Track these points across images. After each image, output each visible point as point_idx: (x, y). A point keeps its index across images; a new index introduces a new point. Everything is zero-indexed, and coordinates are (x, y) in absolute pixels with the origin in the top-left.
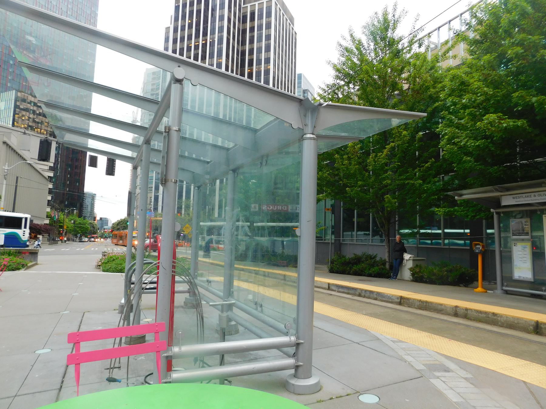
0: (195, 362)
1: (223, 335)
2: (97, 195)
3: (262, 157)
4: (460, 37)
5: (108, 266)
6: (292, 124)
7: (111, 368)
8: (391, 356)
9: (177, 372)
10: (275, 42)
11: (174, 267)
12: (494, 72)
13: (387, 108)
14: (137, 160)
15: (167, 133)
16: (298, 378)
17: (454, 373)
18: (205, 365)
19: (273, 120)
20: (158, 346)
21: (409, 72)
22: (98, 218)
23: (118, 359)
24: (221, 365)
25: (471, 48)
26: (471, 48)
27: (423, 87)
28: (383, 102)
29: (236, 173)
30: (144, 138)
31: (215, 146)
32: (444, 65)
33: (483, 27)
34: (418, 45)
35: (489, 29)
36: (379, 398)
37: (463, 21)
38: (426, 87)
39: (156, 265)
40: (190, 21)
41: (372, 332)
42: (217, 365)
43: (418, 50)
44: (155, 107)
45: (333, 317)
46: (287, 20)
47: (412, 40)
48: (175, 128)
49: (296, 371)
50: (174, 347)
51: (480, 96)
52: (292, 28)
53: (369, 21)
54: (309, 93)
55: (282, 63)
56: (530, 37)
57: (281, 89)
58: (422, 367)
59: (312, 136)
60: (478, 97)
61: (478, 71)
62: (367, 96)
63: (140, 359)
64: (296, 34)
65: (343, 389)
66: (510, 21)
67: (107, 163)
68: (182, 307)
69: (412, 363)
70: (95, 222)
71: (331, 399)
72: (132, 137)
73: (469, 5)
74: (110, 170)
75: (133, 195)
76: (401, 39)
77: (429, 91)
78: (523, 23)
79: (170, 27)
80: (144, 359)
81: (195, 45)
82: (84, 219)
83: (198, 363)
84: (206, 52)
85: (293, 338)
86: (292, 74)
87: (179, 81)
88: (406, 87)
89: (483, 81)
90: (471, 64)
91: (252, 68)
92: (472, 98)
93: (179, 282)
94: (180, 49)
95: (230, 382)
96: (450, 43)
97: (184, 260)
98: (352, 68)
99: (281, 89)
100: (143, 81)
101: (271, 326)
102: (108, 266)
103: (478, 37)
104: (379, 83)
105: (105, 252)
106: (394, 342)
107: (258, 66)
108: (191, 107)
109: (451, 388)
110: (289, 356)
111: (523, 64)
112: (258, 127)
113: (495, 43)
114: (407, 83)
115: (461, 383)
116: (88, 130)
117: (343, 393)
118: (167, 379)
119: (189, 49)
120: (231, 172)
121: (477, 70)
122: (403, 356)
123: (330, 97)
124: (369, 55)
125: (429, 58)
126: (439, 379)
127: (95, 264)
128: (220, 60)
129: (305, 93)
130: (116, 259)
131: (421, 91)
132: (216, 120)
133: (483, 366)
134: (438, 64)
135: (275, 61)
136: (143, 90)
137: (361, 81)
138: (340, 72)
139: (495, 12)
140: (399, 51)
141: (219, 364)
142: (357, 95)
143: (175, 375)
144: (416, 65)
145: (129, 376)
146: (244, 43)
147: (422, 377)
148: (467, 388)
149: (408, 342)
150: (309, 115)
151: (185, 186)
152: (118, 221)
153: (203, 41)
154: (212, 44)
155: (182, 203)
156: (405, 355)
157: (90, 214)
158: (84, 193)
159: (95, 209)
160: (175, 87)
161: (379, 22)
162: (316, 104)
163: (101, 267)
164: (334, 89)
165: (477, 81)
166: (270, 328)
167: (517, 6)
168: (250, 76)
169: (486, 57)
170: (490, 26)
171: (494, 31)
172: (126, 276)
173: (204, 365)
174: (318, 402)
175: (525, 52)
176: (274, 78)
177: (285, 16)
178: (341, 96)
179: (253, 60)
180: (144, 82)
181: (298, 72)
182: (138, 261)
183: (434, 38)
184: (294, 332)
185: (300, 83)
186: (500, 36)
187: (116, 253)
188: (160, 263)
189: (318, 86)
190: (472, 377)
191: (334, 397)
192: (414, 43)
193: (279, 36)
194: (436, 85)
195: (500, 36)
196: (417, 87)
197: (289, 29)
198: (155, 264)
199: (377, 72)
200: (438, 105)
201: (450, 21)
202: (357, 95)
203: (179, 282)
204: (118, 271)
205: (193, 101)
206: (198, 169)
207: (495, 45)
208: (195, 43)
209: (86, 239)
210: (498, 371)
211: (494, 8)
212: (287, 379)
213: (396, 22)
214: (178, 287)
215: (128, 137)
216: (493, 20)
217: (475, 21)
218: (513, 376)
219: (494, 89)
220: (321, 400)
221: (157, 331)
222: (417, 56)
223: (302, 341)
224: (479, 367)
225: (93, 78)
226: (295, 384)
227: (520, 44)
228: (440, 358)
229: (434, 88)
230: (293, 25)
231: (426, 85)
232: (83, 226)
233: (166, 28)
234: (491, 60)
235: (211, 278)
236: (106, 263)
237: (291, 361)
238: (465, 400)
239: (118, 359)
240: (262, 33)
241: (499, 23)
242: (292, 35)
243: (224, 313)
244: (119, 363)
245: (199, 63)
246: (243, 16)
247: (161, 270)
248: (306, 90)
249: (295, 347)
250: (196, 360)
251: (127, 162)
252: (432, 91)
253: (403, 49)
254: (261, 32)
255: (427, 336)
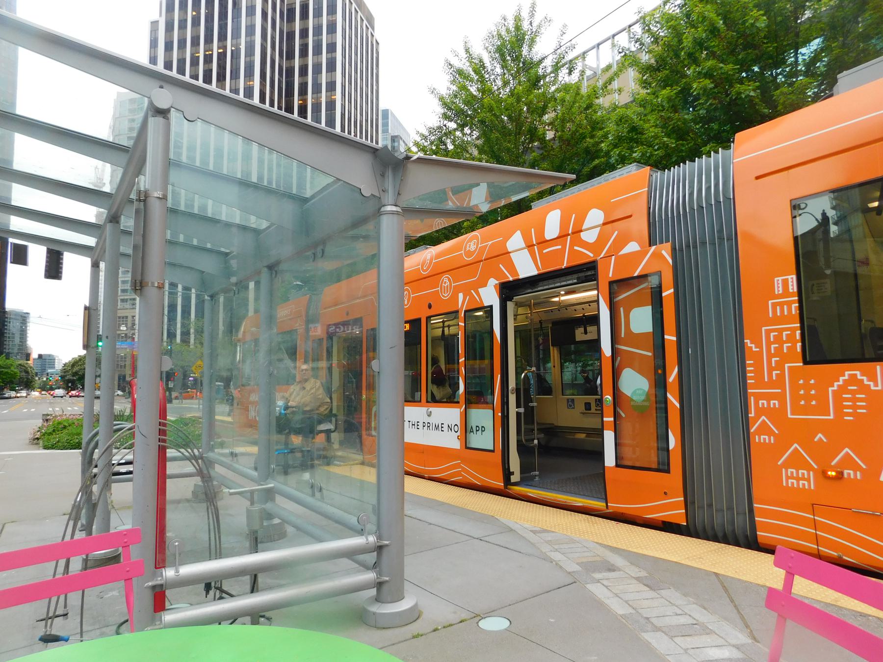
0: (207, 592)
1: (255, 545)
2: (31, 315)
3: (315, 245)
4: (628, 60)
5: (54, 439)
6: (361, 188)
7: (49, 618)
8: (530, 555)
9: (173, 611)
10: (344, 56)
11: (162, 432)
12: (677, 114)
13: (523, 166)
14: (98, 251)
15: (142, 203)
16: (383, 603)
17: (622, 572)
18: (224, 595)
19: (332, 182)
20: (128, 569)
21: (555, 112)
22: (34, 355)
23: (62, 597)
24: (252, 591)
25: (645, 78)
26: (645, 78)
27: (575, 135)
28: (517, 157)
29: (274, 272)
30: (108, 212)
31: (244, 228)
32: (604, 102)
33: (660, 48)
34: (567, 71)
35: (668, 50)
36: (510, 622)
37: (632, 36)
38: (581, 134)
39: (130, 431)
40: (194, 13)
41: (502, 520)
42: (247, 593)
43: (567, 79)
44: (124, 158)
45: (442, 500)
46: (362, 20)
47: (557, 63)
48: (156, 195)
49: (378, 591)
50: (166, 569)
51: (658, 149)
52: (371, 33)
53: (493, 29)
54: (400, 140)
55: (356, 90)
56: (721, 65)
57: (361, 137)
58: (577, 568)
59: (394, 208)
60: (656, 150)
61: (653, 112)
62: (491, 147)
63: (109, 595)
64: (378, 44)
65: (455, 613)
66: (695, 39)
67: (47, 257)
68: (188, 501)
69: (561, 564)
70: (29, 362)
71: (435, 630)
72: (95, 213)
73: (640, 12)
74: (54, 270)
75: (92, 312)
76: (541, 61)
77: (585, 142)
78: (713, 44)
79: (158, 21)
80: (118, 594)
81: (205, 56)
82: (7, 359)
83: (212, 593)
84: (225, 69)
85: (372, 539)
86: (372, 109)
87: (163, 113)
88: (550, 135)
89: (661, 127)
90: (645, 101)
91: (304, 97)
92: (646, 152)
93: (174, 459)
94: (179, 61)
95: (269, 619)
96: (615, 68)
97: (194, 421)
98: (467, 103)
99: (361, 137)
100: (112, 114)
101: (337, 522)
102: (54, 439)
103: (653, 61)
104: (510, 127)
105: (48, 415)
106: (534, 532)
107: (315, 95)
108: (188, 157)
109: (617, 595)
110: (366, 567)
111: (714, 104)
112: (308, 193)
113: (678, 72)
114: (551, 130)
115: (631, 586)
116: (10, 199)
117: (453, 618)
118: (156, 624)
119: (195, 62)
120: (266, 269)
121: (652, 111)
122: (548, 554)
123: (434, 148)
124: (493, 83)
125: (584, 91)
126: (599, 584)
127: (29, 435)
128: (251, 83)
129: (394, 142)
130: (70, 426)
131: (572, 142)
132: (245, 184)
133: (663, 557)
134: (597, 101)
135: (343, 87)
136: (113, 130)
137: (482, 122)
138: (450, 109)
139: (675, 26)
140: (538, 79)
141: (248, 588)
142: (476, 146)
143: (168, 617)
144: (565, 101)
145: (85, 628)
146: (290, 56)
147: (575, 582)
148: (638, 592)
149: (557, 531)
150: (390, 174)
151: (193, 297)
152: (73, 359)
153: (219, 48)
154: (236, 55)
155: (189, 324)
156: (551, 551)
157: (19, 349)
158: (5, 312)
159: (28, 339)
160: (154, 123)
161: (508, 31)
162: (401, 157)
163: (41, 442)
164: (442, 135)
165: (653, 126)
166: (337, 525)
167: (704, 18)
168: (303, 112)
169: (666, 92)
170: (668, 46)
171: (674, 55)
172: (84, 455)
173: (223, 594)
174: (414, 637)
175: (716, 87)
176: (343, 115)
177: (359, 13)
178: (451, 147)
179: (306, 83)
180: (114, 115)
181: (382, 106)
182: (102, 428)
183: (591, 60)
184: (374, 528)
185: (385, 125)
186: (682, 62)
187: (70, 415)
188: (136, 427)
189: (415, 131)
190: (647, 575)
191: (440, 628)
192: (561, 67)
193: (350, 47)
194: (594, 133)
195: (682, 62)
196: (567, 135)
197: (367, 35)
198: (130, 429)
199: (506, 110)
200: (598, 163)
201: (614, 36)
202: (476, 146)
203: (174, 459)
204: (74, 447)
205: (191, 148)
206: (209, 265)
207: (677, 74)
208: (205, 51)
209: (13, 394)
210: (683, 562)
211: (673, 20)
212: (365, 606)
213: (535, 35)
214: (171, 468)
215: (88, 213)
216: (673, 37)
217: (649, 37)
218: (702, 567)
219: (677, 139)
220: (420, 633)
221: (126, 545)
222: (566, 88)
223: (387, 542)
224: (656, 560)
225: (14, 104)
226: (377, 611)
227: (708, 75)
228: (601, 551)
229: (592, 137)
230: (373, 29)
231: (581, 131)
232: (6, 370)
233: (152, 23)
234: (672, 96)
235: (239, 450)
236: (50, 434)
237: (370, 576)
238: (635, 610)
239: (62, 597)
240: (322, 40)
241: (680, 41)
242: (372, 45)
243: (256, 505)
244: (65, 606)
245: (213, 87)
246: (288, 10)
247: (138, 439)
248: (396, 137)
249: (376, 553)
250: (208, 587)
251: (82, 255)
252: (590, 142)
253: (544, 76)
254: (320, 37)
255: (584, 520)
